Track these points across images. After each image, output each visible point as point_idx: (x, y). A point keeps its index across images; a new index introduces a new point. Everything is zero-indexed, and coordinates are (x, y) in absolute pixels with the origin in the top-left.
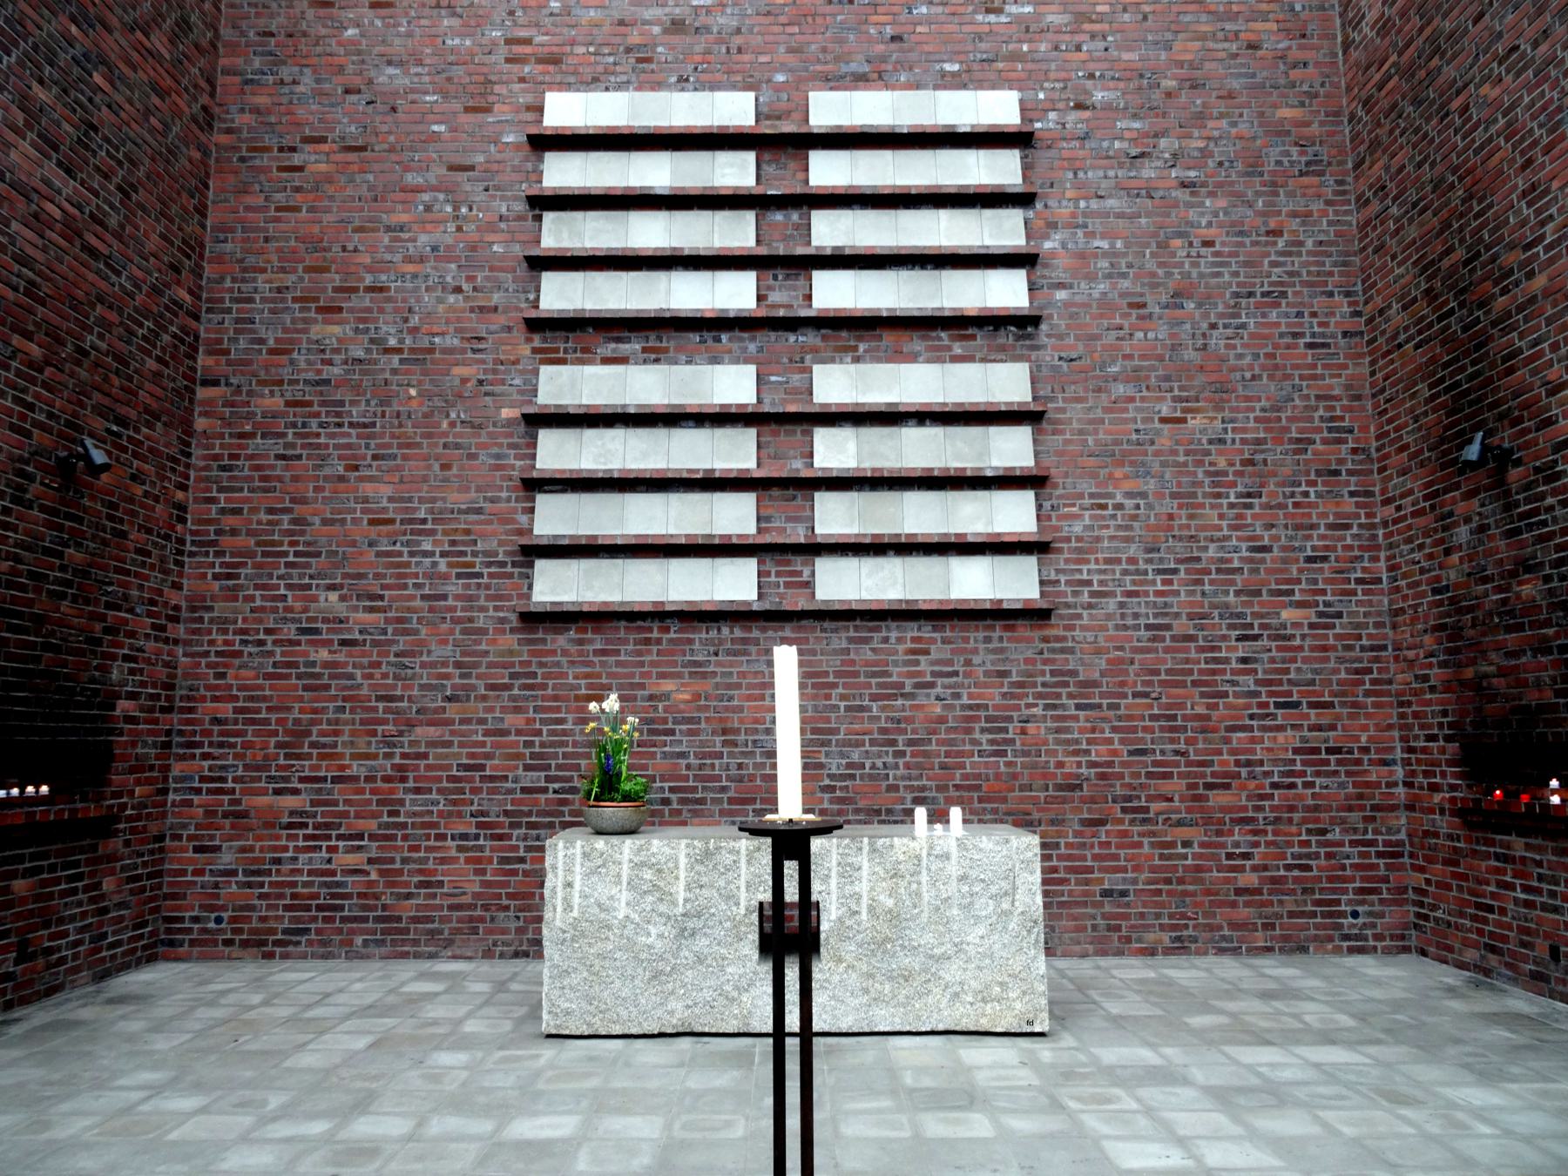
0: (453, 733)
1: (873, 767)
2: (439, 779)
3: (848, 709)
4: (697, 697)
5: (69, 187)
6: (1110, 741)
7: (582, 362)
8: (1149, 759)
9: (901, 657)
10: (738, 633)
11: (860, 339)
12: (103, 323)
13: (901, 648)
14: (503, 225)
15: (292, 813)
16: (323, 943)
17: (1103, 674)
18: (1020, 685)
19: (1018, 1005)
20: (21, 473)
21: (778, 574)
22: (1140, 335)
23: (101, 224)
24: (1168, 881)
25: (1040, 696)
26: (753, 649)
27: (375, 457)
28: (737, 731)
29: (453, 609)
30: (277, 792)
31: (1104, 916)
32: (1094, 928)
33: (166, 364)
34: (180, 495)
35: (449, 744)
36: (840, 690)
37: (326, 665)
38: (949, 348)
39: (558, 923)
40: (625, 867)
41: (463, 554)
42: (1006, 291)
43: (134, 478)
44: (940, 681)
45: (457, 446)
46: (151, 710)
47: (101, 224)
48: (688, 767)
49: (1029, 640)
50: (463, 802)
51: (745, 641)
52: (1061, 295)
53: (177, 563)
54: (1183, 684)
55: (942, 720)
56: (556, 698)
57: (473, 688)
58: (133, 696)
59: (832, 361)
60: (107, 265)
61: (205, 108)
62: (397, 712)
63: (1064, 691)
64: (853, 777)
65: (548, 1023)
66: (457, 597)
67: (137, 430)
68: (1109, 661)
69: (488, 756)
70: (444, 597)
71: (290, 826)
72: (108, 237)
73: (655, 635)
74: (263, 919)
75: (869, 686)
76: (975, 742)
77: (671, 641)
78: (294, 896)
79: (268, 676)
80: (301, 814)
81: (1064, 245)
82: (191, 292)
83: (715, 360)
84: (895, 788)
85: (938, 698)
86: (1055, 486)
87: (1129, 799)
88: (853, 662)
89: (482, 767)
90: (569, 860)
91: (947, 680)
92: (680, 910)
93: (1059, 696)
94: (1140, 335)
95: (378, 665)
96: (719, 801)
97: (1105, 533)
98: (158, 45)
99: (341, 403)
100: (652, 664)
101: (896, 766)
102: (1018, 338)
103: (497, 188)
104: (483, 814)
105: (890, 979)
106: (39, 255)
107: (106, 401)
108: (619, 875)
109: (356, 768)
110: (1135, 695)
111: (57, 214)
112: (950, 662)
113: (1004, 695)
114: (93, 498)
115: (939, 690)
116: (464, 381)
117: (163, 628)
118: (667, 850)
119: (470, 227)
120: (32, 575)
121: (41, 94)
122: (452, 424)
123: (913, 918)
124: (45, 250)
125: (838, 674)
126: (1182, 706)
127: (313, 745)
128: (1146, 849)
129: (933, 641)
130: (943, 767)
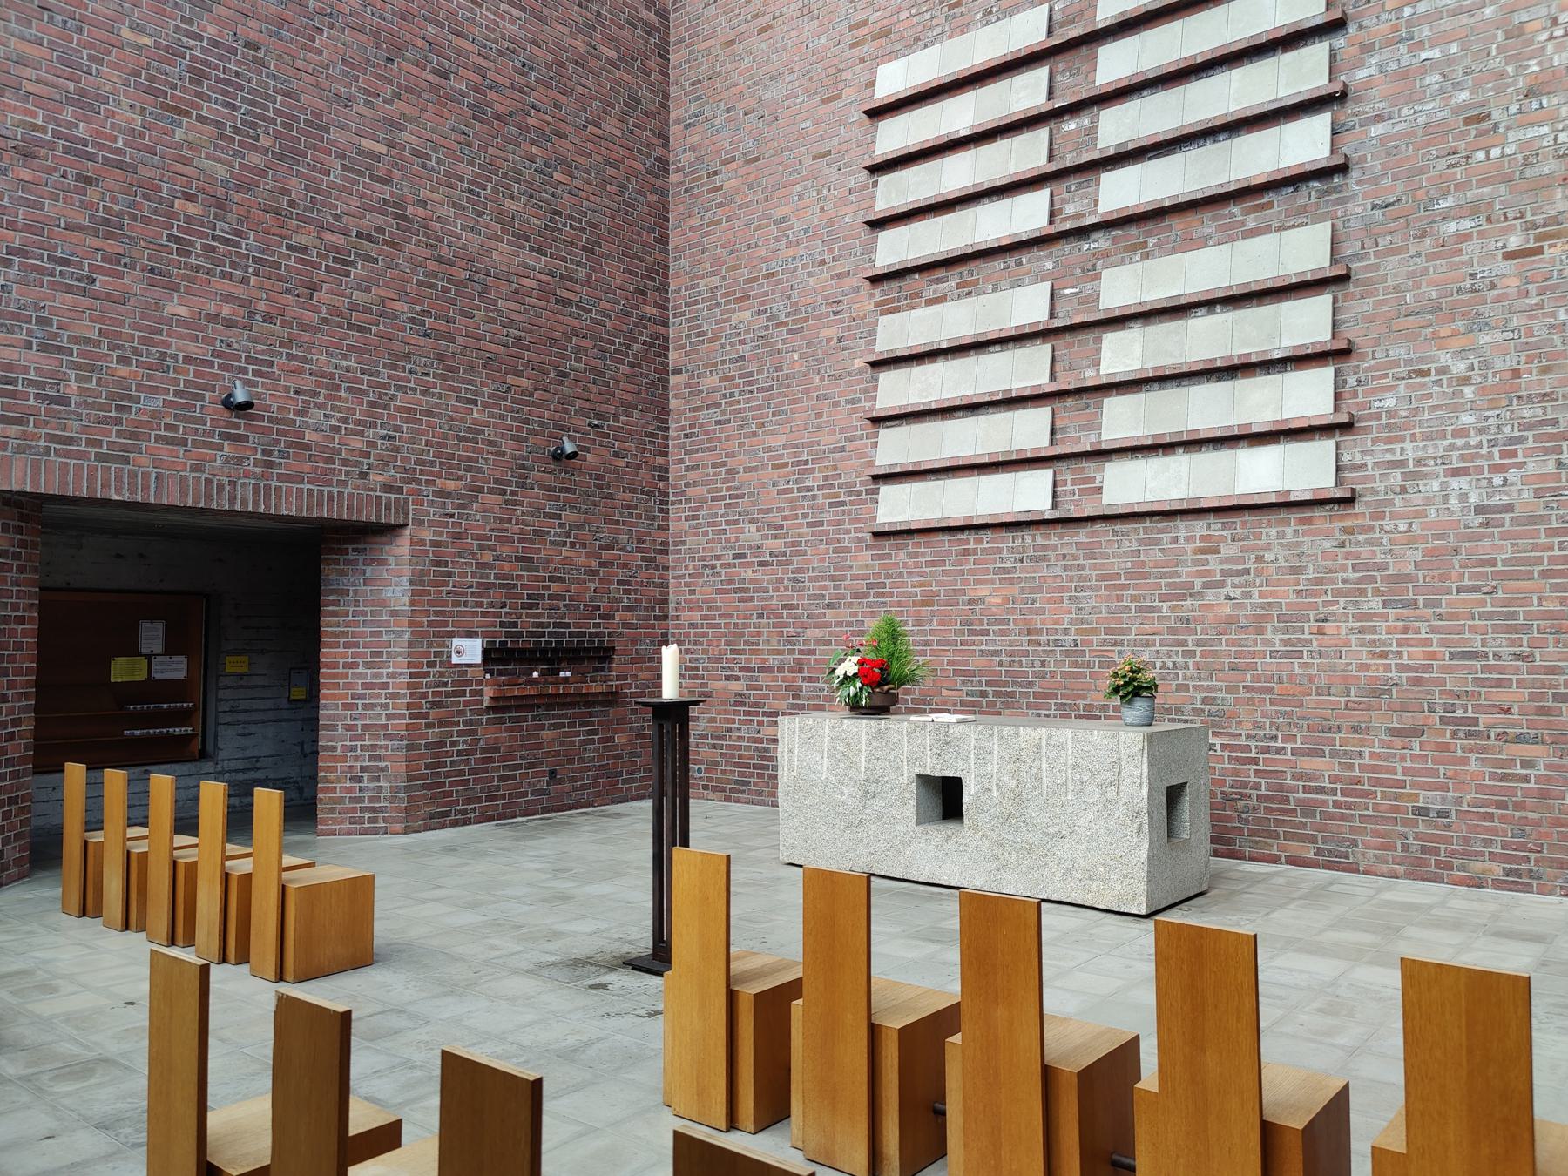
3: (1139, 609)
4: (1007, 600)
5: (542, 262)
7: (912, 307)
9: (1190, 557)
10: (1039, 541)
11: (1149, 234)
12: (578, 350)
13: (1190, 547)
14: (852, 198)
15: (737, 695)
16: (759, 793)
19: (1118, 887)
20: (523, 467)
21: (1073, 482)
22: (1481, 155)
23: (571, 280)
24: (1502, 805)
26: (1052, 555)
27: (774, 415)
29: (826, 533)
30: (728, 678)
31: (1417, 837)
32: (1405, 848)
33: (639, 366)
34: (660, 460)
37: (752, 581)
38: (1243, 223)
41: (833, 486)
42: (1306, 143)
43: (616, 455)
44: (1229, 580)
45: (826, 397)
46: (648, 618)
47: (571, 280)
49: (1328, 534)
51: (1045, 548)
52: (1377, 130)
53: (661, 511)
54: (1529, 576)
55: (1231, 620)
57: (844, 596)
58: (629, 609)
59: (1123, 262)
60: (578, 307)
61: (658, 159)
62: (795, 617)
66: (830, 523)
67: (616, 420)
70: (821, 523)
71: (736, 704)
72: (578, 287)
73: (972, 546)
74: (724, 772)
75: (1159, 587)
77: (983, 550)
78: (740, 757)
79: (719, 591)
80: (743, 695)
81: (1381, 69)
82: (657, 306)
83: (1017, 284)
85: (1228, 598)
86: (1363, 357)
88: (1143, 564)
91: (1237, 580)
92: (863, 776)
94: (1481, 155)
95: (780, 580)
97: (1426, 403)
98: (608, 128)
99: (751, 374)
100: (971, 572)
101: (1186, 666)
102: (1323, 194)
103: (847, 165)
106: (521, 317)
107: (587, 404)
108: (821, 746)
109: (772, 662)
111: (533, 284)
114: (581, 474)
115: (1228, 590)
116: (829, 340)
117: (653, 559)
118: (853, 728)
119: (829, 206)
120: (536, 532)
121: (511, 206)
122: (822, 379)
124: (526, 312)
126: (1526, 601)
127: (746, 643)
128: (1474, 766)
129: (1223, 539)
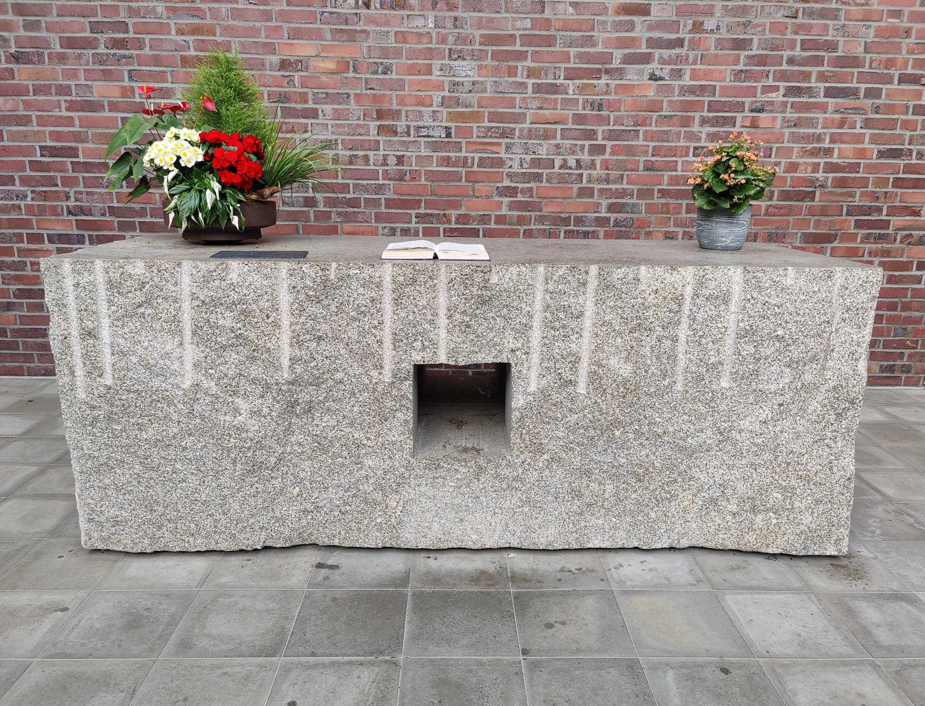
0: (27, 105)
1: (564, 165)
2: (21, 166)
4: (344, 66)
6: (859, 139)
8: (901, 162)
17: (867, 50)
18: (762, 60)
19: (807, 519)
25: (783, 76)
28: (396, 115)
35: (26, 120)
36: (529, 63)
39: (82, 395)
40: (186, 305)
44: (657, 53)
48: (336, 161)
50: (55, 196)
55: (654, 106)
56: (156, 60)
63: (814, 70)
64: (538, 177)
65: (89, 534)
68: (879, 32)
69: (77, 137)
76: (692, 137)
84: (586, 192)
85: (653, 77)
87: (868, 211)
89: (73, 152)
90: (86, 292)
91: (666, 53)
93: (807, 76)
96: (375, 203)
104: (82, 211)
105: (615, 477)
110: (903, 79)
112: (672, 26)
113: (738, 74)
115: (654, 66)
123: (660, 393)
125: (528, 40)
130: (650, 167)
